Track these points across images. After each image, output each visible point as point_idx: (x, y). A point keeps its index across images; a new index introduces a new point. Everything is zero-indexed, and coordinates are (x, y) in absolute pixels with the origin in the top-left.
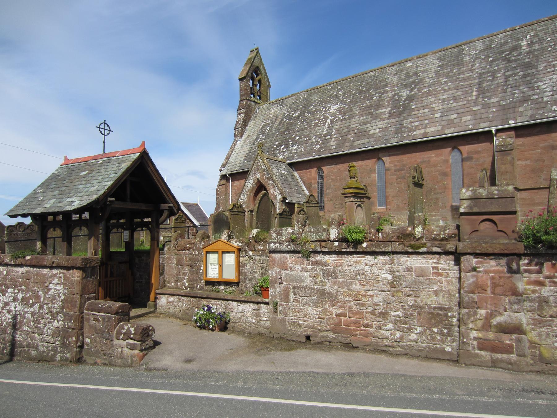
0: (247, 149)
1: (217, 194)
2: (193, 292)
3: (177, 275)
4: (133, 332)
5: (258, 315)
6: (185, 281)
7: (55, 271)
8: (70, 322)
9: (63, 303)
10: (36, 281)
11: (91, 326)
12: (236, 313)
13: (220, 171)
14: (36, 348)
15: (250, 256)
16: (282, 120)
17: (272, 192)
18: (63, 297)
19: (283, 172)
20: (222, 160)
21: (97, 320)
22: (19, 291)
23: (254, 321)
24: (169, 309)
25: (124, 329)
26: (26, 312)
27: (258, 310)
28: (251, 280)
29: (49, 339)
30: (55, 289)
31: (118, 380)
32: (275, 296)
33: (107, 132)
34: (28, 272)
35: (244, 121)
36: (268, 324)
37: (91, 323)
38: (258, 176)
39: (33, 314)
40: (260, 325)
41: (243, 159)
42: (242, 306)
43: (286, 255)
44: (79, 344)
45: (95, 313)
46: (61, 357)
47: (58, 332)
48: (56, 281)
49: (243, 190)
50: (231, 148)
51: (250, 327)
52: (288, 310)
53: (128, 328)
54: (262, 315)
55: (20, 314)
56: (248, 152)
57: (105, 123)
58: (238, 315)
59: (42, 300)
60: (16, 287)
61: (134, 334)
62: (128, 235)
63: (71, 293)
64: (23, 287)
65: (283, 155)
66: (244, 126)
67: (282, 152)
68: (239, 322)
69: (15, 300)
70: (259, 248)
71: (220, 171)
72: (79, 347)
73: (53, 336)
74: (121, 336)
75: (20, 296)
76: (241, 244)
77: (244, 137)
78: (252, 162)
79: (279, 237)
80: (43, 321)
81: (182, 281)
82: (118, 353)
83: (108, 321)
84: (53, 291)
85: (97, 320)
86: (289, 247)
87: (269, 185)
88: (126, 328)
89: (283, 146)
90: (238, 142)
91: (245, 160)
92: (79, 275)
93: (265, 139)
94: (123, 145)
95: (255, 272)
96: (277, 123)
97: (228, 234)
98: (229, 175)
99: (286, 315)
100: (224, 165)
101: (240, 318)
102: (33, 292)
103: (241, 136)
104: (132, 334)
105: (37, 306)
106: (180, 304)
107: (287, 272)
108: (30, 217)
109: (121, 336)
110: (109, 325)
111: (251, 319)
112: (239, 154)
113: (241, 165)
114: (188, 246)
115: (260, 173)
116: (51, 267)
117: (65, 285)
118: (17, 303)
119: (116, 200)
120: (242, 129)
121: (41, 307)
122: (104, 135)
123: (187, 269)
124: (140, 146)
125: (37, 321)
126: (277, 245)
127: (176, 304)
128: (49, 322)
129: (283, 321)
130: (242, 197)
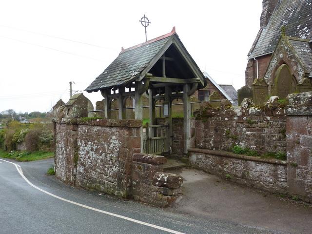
0: (272, 34)
1: (246, 75)
2: (217, 152)
3: (205, 137)
4: (166, 181)
5: (275, 176)
6: (211, 142)
7: (114, 130)
8: (123, 168)
9: (119, 154)
10: (103, 137)
11: (136, 173)
12: (255, 172)
13: (248, 56)
14: (104, 184)
15: (268, 121)
16: (305, 4)
17: (295, 69)
18: (118, 150)
19: (306, 50)
20: (250, 46)
21: (140, 168)
22: (94, 144)
23: (271, 180)
24: (198, 164)
25: (159, 177)
26: (98, 159)
27: (276, 170)
28: (269, 143)
29: (111, 179)
30: (114, 143)
31: (150, 217)
32: (293, 159)
33: (147, 24)
34: (98, 130)
35: (269, 11)
36: (285, 185)
37: (136, 170)
38: (281, 55)
39: (102, 160)
40: (277, 185)
41: (268, 43)
42: (260, 167)
43: (304, 119)
44: (128, 185)
45: (138, 162)
46: (118, 193)
47: (115, 174)
48: (114, 137)
49: (267, 70)
50: (257, 36)
51: (268, 186)
52: (307, 173)
53: (163, 177)
54: (280, 176)
55: (95, 160)
56: (272, 37)
57: (145, 17)
58: (257, 174)
59: (106, 151)
60: (92, 141)
61: (167, 182)
62: (100, 93)
63: (123, 147)
64: (96, 141)
65: (306, 36)
66: (269, 15)
67: (304, 33)
68: (257, 180)
69: (92, 150)
70: (277, 113)
71: (248, 56)
72: (129, 187)
73: (113, 178)
74: (157, 183)
75: (95, 147)
76: (259, 110)
77: (268, 26)
78: (275, 46)
79: (297, 101)
80: (107, 166)
81: (208, 141)
82: (154, 195)
83: (147, 170)
84: (112, 144)
85: (140, 168)
86: (307, 111)
87: (292, 63)
88: (161, 176)
89: (306, 28)
90: (264, 30)
91: (270, 44)
92: (127, 133)
93: (288, 24)
94: (159, 30)
95: (274, 136)
96: (300, 8)
97: (248, 101)
98: (256, 58)
99: (304, 178)
100: (252, 51)
101: (258, 177)
102: (102, 144)
103: (266, 25)
104: (165, 182)
105: (104, 154)
106: (207, 160)
107: (305, 136)
108: (99, 91)
109: (157, 183)
110: (148, 173)
111: (269, 179)
112: (264, 40)
113: (267, 49)
114: (213, 112)
115: (283, 53)
116: (111, 127)
117: (119, 140)
118: (93, 152)
119: (153, 76)
120: (267, 19)
121: (106, 156)
122: (145, 27)
123: (212, 132)
124: (172, 31)
125: (104, 166)
126: (295, 109)
127: (203, 161)
128: (111, 167)
129: (302, 183)
130: (267, 76)
